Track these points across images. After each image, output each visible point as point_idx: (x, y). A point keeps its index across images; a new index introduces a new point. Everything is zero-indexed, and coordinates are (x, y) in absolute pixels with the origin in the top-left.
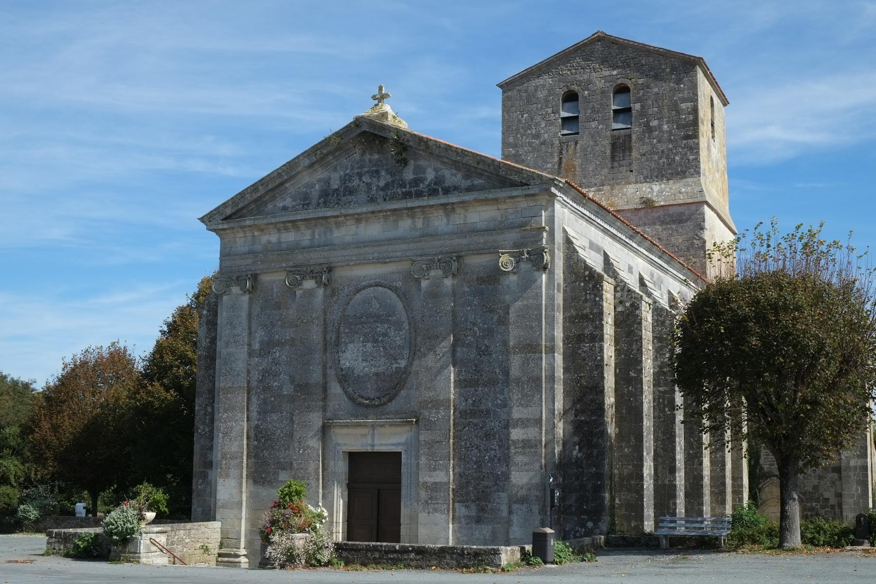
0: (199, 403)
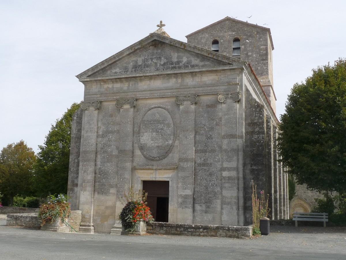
0: (72, 158)
